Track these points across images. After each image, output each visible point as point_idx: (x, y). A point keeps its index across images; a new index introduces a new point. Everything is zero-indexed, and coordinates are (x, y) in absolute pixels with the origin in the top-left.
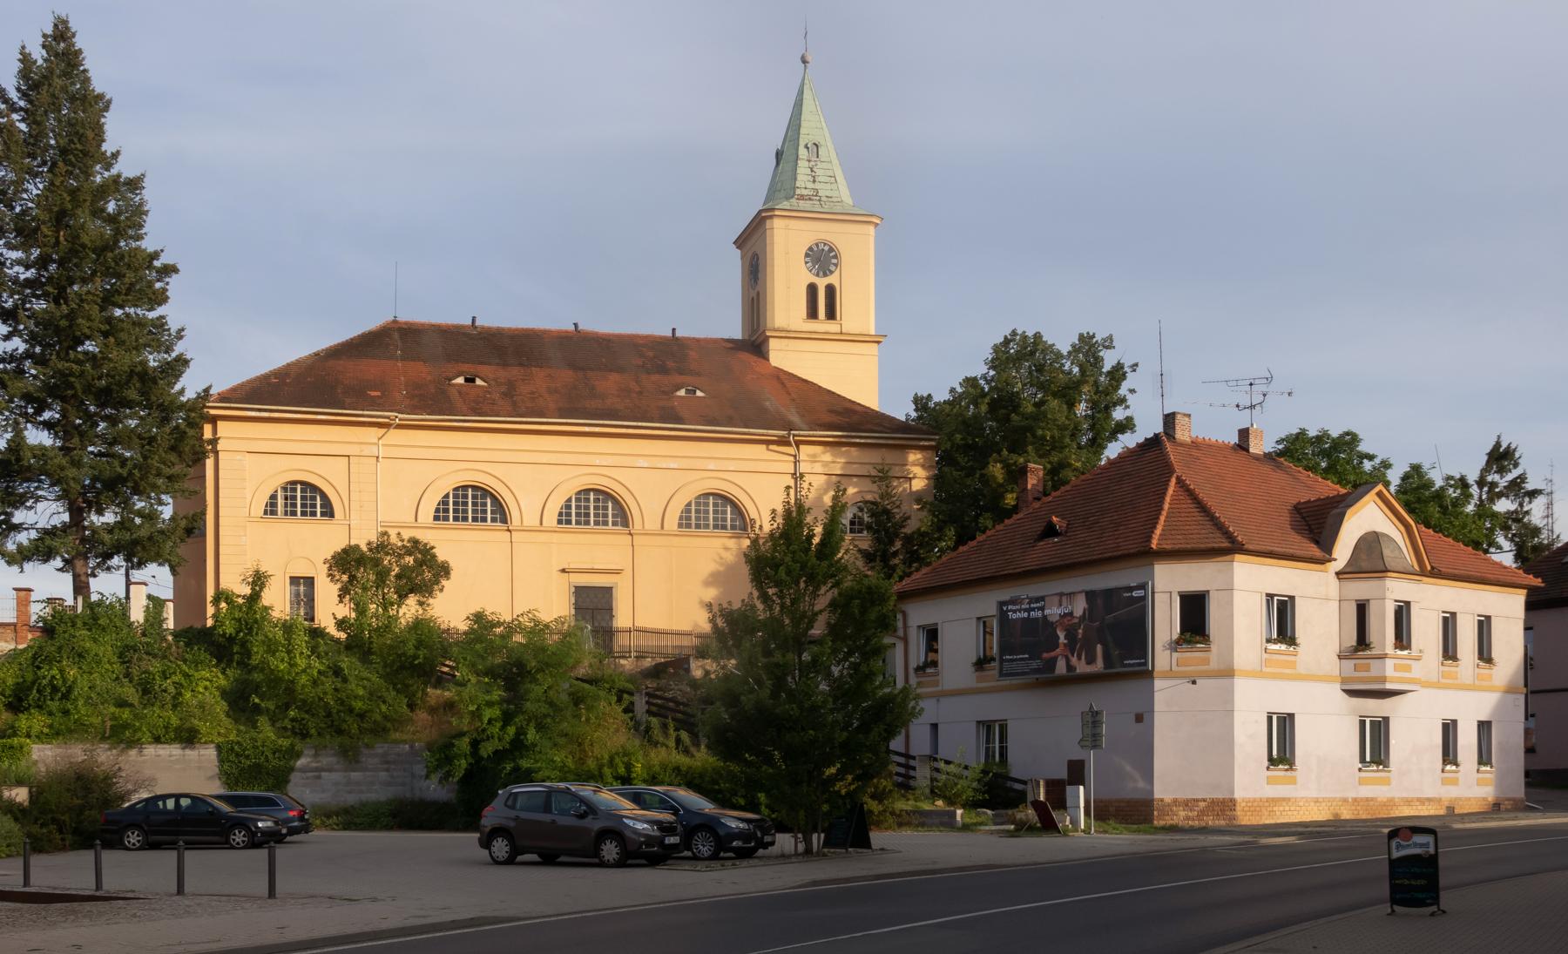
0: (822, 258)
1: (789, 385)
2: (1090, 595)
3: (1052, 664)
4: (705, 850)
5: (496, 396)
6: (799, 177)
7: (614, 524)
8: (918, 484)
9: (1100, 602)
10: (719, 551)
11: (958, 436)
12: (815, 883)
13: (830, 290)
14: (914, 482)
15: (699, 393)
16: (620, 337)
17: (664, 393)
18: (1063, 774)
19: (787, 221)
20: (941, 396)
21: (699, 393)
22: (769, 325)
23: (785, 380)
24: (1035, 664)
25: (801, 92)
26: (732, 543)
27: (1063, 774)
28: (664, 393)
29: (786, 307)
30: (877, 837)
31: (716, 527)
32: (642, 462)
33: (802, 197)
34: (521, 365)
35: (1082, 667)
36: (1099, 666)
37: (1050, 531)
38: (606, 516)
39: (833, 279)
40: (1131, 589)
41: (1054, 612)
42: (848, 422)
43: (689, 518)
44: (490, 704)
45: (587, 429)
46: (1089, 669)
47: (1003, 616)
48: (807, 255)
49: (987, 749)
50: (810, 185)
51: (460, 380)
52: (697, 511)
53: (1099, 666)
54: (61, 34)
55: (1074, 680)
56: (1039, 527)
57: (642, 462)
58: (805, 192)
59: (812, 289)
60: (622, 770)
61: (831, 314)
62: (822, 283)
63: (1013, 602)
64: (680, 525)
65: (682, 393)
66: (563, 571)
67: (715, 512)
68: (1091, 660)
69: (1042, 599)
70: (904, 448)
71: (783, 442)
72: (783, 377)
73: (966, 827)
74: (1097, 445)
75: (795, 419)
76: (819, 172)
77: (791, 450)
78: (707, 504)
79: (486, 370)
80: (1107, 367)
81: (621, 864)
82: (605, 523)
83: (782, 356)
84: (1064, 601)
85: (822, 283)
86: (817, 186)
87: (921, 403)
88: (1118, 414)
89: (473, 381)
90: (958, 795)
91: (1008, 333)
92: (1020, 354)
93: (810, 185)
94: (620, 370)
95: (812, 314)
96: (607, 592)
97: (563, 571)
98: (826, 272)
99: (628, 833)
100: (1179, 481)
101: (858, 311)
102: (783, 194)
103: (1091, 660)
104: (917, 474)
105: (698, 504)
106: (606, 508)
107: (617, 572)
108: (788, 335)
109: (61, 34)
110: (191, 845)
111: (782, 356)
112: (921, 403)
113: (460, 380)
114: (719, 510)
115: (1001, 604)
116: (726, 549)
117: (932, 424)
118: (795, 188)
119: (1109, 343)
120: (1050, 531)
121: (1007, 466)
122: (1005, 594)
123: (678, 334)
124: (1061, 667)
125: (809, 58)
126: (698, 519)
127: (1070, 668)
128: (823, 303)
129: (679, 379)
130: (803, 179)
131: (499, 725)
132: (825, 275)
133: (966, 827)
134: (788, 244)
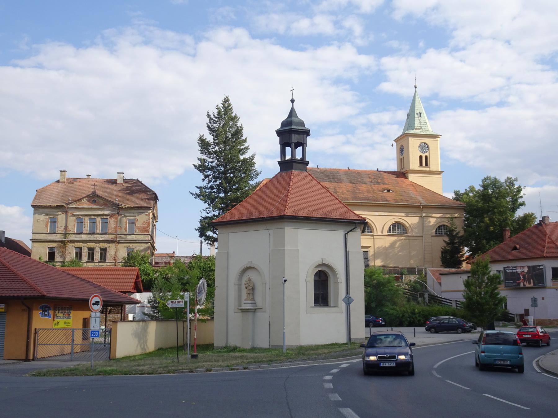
2: (529, 267)
3: (519, 284)
9: (531, 269)
13: (426, 157)
18: (523, 312)
20: (463, 191)
23: (414, 185)
24: (515, 284)
27: (523, 312)
33: (417, 129)
35: (527, 285)
36: (532, 285)
37: (515, 248)
40: (539, 266)
41: (519, 271)
46: (529, 286)
47: (505, 271)
50: (419, 125)
53: (532, 285)
54: (226, 100)
55: (525, 288)
56: (513, 247)
61: (427, 165)
63: (508, 267)
68: (530, 283)
69: (516, 267)
74: (514, 210)
76: (421, 121)
80: (516, 186)
84: (522, 268)
88: (520, 200)
91: (486, 177)
92: (490, 184)
93: (419, 125)
94: (365, 183)
95: (421, 164)
100: (549, 237)
103: (530, 283)
107: (369, 247)
109: (226, 100)
115: (504, 268)
118: (414, 126)
119: (516, 180)
120: (515, 248)
122: (506, 265)
124: (522, 285)
125: (417, 85)
127: (524, 285)
134: (414, 144)
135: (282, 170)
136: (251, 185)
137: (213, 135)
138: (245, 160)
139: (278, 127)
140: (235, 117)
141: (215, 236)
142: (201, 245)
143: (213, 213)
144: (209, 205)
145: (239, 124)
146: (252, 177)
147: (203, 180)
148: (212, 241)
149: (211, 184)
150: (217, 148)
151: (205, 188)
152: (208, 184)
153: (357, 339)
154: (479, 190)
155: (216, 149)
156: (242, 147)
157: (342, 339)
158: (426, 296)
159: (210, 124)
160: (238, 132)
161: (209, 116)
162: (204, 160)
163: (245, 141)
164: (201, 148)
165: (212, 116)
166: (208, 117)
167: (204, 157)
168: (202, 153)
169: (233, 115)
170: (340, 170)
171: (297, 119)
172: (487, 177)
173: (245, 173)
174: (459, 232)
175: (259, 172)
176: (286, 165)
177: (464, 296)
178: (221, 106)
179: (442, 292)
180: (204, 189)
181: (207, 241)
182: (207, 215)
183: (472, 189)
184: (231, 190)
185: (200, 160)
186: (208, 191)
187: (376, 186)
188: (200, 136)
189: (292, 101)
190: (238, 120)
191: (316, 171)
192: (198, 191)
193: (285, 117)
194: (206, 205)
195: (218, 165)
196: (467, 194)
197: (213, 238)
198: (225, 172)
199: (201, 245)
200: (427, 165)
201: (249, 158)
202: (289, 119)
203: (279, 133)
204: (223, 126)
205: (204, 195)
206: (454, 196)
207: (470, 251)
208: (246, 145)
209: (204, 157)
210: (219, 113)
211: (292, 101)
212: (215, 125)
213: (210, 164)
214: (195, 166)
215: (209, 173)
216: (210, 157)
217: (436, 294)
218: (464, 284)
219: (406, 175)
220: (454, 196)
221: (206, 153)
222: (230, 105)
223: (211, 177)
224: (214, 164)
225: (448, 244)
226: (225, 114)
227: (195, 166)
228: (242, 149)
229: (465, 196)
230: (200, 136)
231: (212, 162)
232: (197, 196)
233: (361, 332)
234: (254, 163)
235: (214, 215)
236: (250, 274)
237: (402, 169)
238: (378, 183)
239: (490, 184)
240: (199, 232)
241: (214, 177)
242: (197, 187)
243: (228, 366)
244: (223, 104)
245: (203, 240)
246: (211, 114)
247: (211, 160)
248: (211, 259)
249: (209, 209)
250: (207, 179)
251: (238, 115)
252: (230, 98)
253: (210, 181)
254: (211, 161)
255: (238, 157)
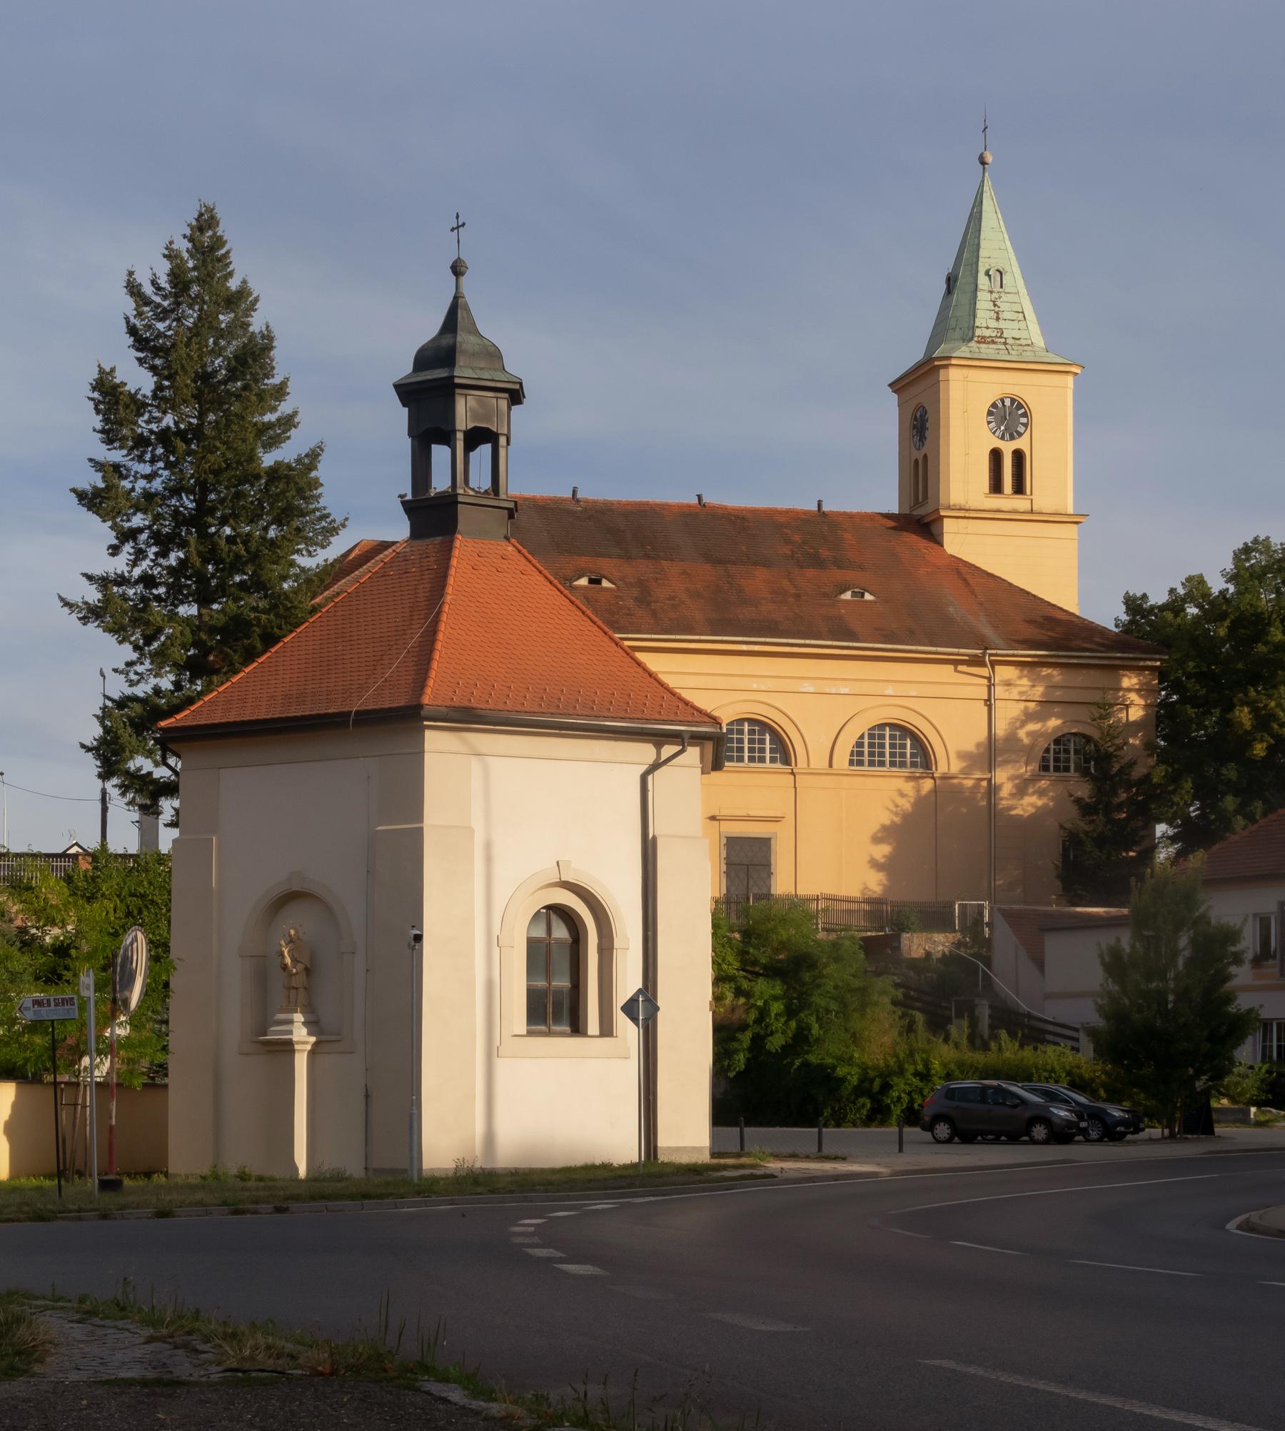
0: (1009, 415)
1: (968, 577)
4: (1094, 1135)
5: (630, 603)
6: (980, 314)
7: (773, 760)
8: (1136, 714)
10: (888, 794)
11: (1191, 664)
12: (1210, 1152)
13: (1018, 456)
14: (1131, 710)
15: (868, 597)
16: (755, 512)
17: (825, 595)
19: (965, 371)
20: (1158, 597)
21: (868, 597)
22: (941, 501)
23: (964, 572)
25: (978, 202)
26: (908, 787)
28: (825, 595)
29: (963, 477)
30: (1218, 1130)
31: (893, 764)
32: (808, 687)
33: (983, 340)
34: (647, 557)
38: (762, 750)
39: (1021, 443)
42: (1055, 638)
43: (861, 754)
44: (775, 998)
45: (744, 647)
48: (990, 413)
49: (1264, 1048)
50: (993, 324)
51: (583, 582)
52: (871, 745)
57: (808, 687)
58: (987, 333)
59: (996, 455)
60: (920, 1067)
61: (1019, 488)
62: (1007, 448)
64: (851, 763)
65: (847, 596)
66: (713, 818)
67: (892, 746)
70: (1115, 669)
71: (977, 662)
72: (964, 570)
73: (1259, 1124)
75: (988, 631)
76: (1003, 306)
77: (985, 671)
78: (882, 737)
79: (606, 565)
81: (1045, 1142)
82: (762, 760)
83: (960, 540)
85: (1007, 448)
86: (1002, 324)
87: (1134, 605)
89: (598, 582)
90: (1241, 1094)
91: (1249, 540)
93: (993, 324)
94: (767, 563)
95: (996, 487)
96: (728, 838)
97: (713, 818)
98: (1013, 435)
99: (1055, 1120)
101: (1054, 481)
102: (958, 333)
104: (1134, 701)
105: (871, 736)
106: (762, 741)
107: (776, 820)
108: (966, 513)
110: (749, 1123)
111: (960, 540)
112: (1134, 605)
113: (583, 582)
114: (897, 745)
116: (902, 795)
117: (1150, 633)
118: (973, 328)
121: (1255, 711)
123: (825, 508)
126: (871, 754)
128: (1008, 473)
129: (841, 575)
130: (984, 316)
131: (783, 1020)
132: (1012, 438)
133: (1259, 1124)
134: (967, 397)
135: (416, 534)
136: (303, 570)
137: (153, 369)
138: (275, 473)
139: (404, 368)
140: (243, 293)
141: (161, 773)
142: (105, 810)
143: (153, 681)
144: (136, 648)
145: (257, 323)
146: (309, 541)
147: (114, 550)
148: (148, 794)
149: (145, 564)
150: (169, 420)
151: (122, 580)
152: (134, 564)
153: (678, 1149)
154: (1223, 593)
155: (164, 424)
156: (270, 417)
157: (622, 1146)
158: (984, 1012)
159: (138, 323)
160: (254, 356)
161: (133, 289)
162: (116, 467)
163: (280, 392)
164: (106, 420)
165: (148, 290)
166: (132, 294)
167: (117, 456)
168: (109, 441)
169: (233, 284)
170: (665, 507)
171: (472, 339)
172: (1256, 541)
173: (278, 521)
174: (1132, 764)
175: (339, 520)
176: (433, 515)
177: (1100, 1009)
178: (183, 246)
179: (1047, 996)
180: (119, 585)
181: (130, 796)
182: (129, 691)
183: (1196, 585)
184: (222, 590)
185: (99, 466)
186: (131, 592)
187: (811, 573)
188: (101, 371)
189: (457, 269)
190: (252, 307)
191: (570, 513)
192: (93, 595)
193: (428, 328)
194: (127, 652)
195: (175, 491)
196: (1176, 605)
197: (156, 782)
198: (197, 520)
199: (105, 810)
200: (1019, 488)
201: (299, 461)
202: (447, 340)
203: (406, 392)
204: (196, 332)
205: (113, 610)
206: (1125, 618)
207: (1173, 839)
208: (285, 408)
209: (117, 456)
210: (177, 277)
211: (457, 269)
212: (161, 326)
213: (141, 483)
214: (81, 496)
215: (138, 520)
216: (140, 459)
217: (1024, 1007)
218: (1103, 963)
219: (934, 529)
220: (1125, 618)
221: (124, 438)
222: (219, 242)
223: (143, 537)
224: (157, 485)
225: (1086, 809)
226: (201, 281)
227: (81, 496)
228: (270, 426)
229: (1169, 616)
230: (101, 371)
231: (149, 478)
232: (92, 613)
233: (688, 1129)
234: (316, 484)
235: (157, 691)
236: (295, 923)
237: (917, 503)
238: (818, 563)
239: (1266, 570)
240: (98, 756)
241: (157, 538)
242: (90, 578)
243: (224, 1203)
244: (191, 240)
245: (114, 793)
246: (144, 280)
247: (146, 469)
248: (147, 864)
249: (140, 668)
250: (128, 547)
251: (256, 288)
252: (219, 213)
253: (139, 555)
254: (146, 476)
255: (252, 458)
